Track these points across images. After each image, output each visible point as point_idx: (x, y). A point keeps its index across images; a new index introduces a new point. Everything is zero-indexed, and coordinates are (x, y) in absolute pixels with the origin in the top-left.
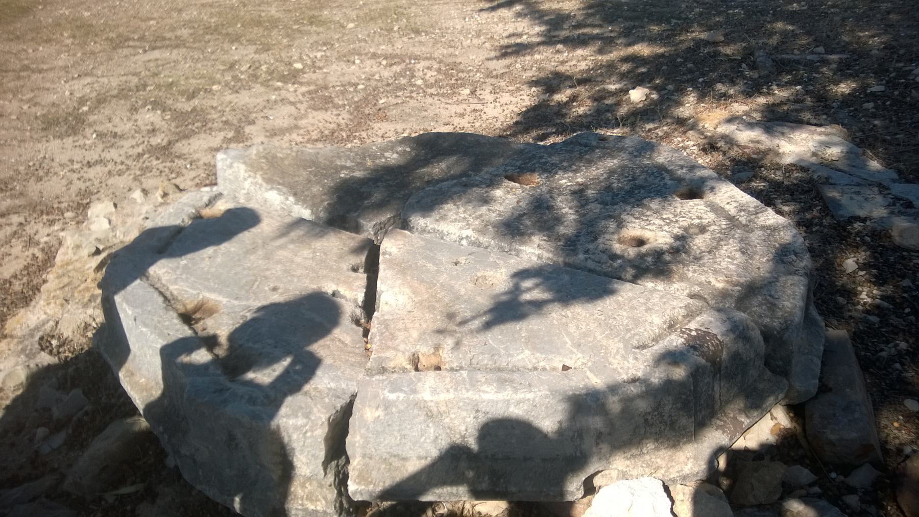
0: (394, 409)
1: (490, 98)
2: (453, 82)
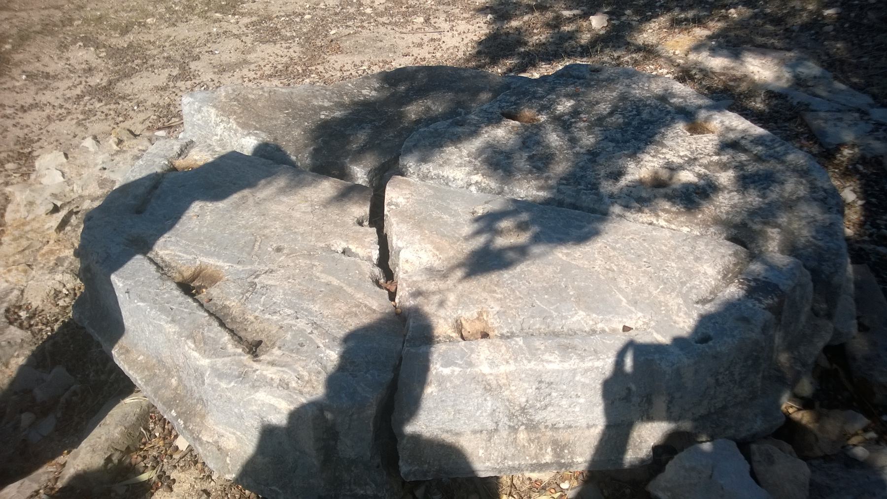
0: (448, 384)
1: (446, 26)
2: (404, 9)
